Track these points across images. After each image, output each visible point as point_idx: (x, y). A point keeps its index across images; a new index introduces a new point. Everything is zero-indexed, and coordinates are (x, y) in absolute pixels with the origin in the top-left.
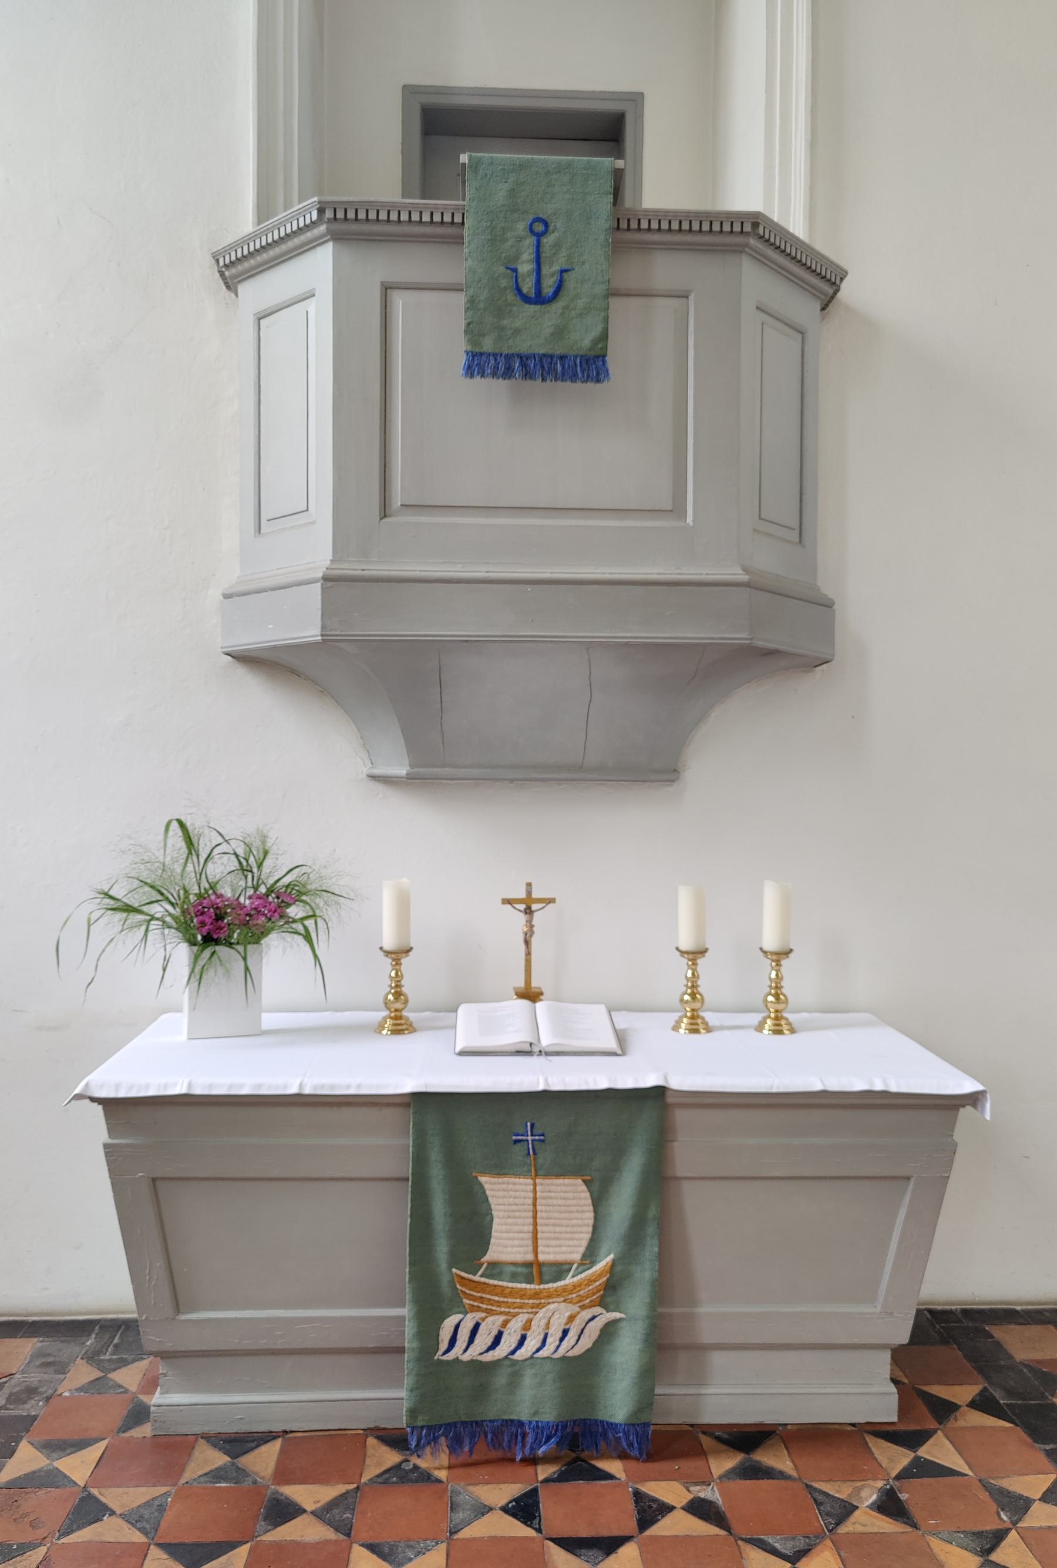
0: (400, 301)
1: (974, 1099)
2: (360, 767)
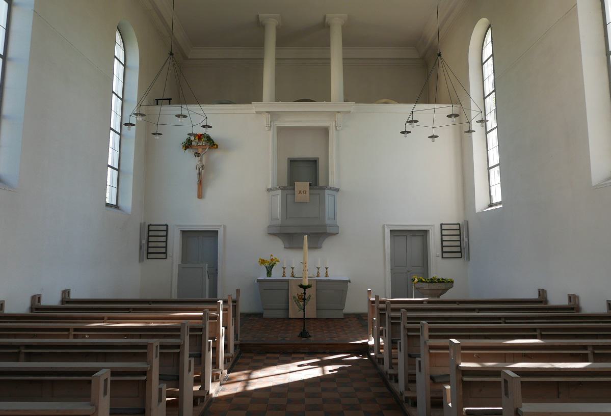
0: (288, 196)
1: (349, 281)
2: (283, 246)
